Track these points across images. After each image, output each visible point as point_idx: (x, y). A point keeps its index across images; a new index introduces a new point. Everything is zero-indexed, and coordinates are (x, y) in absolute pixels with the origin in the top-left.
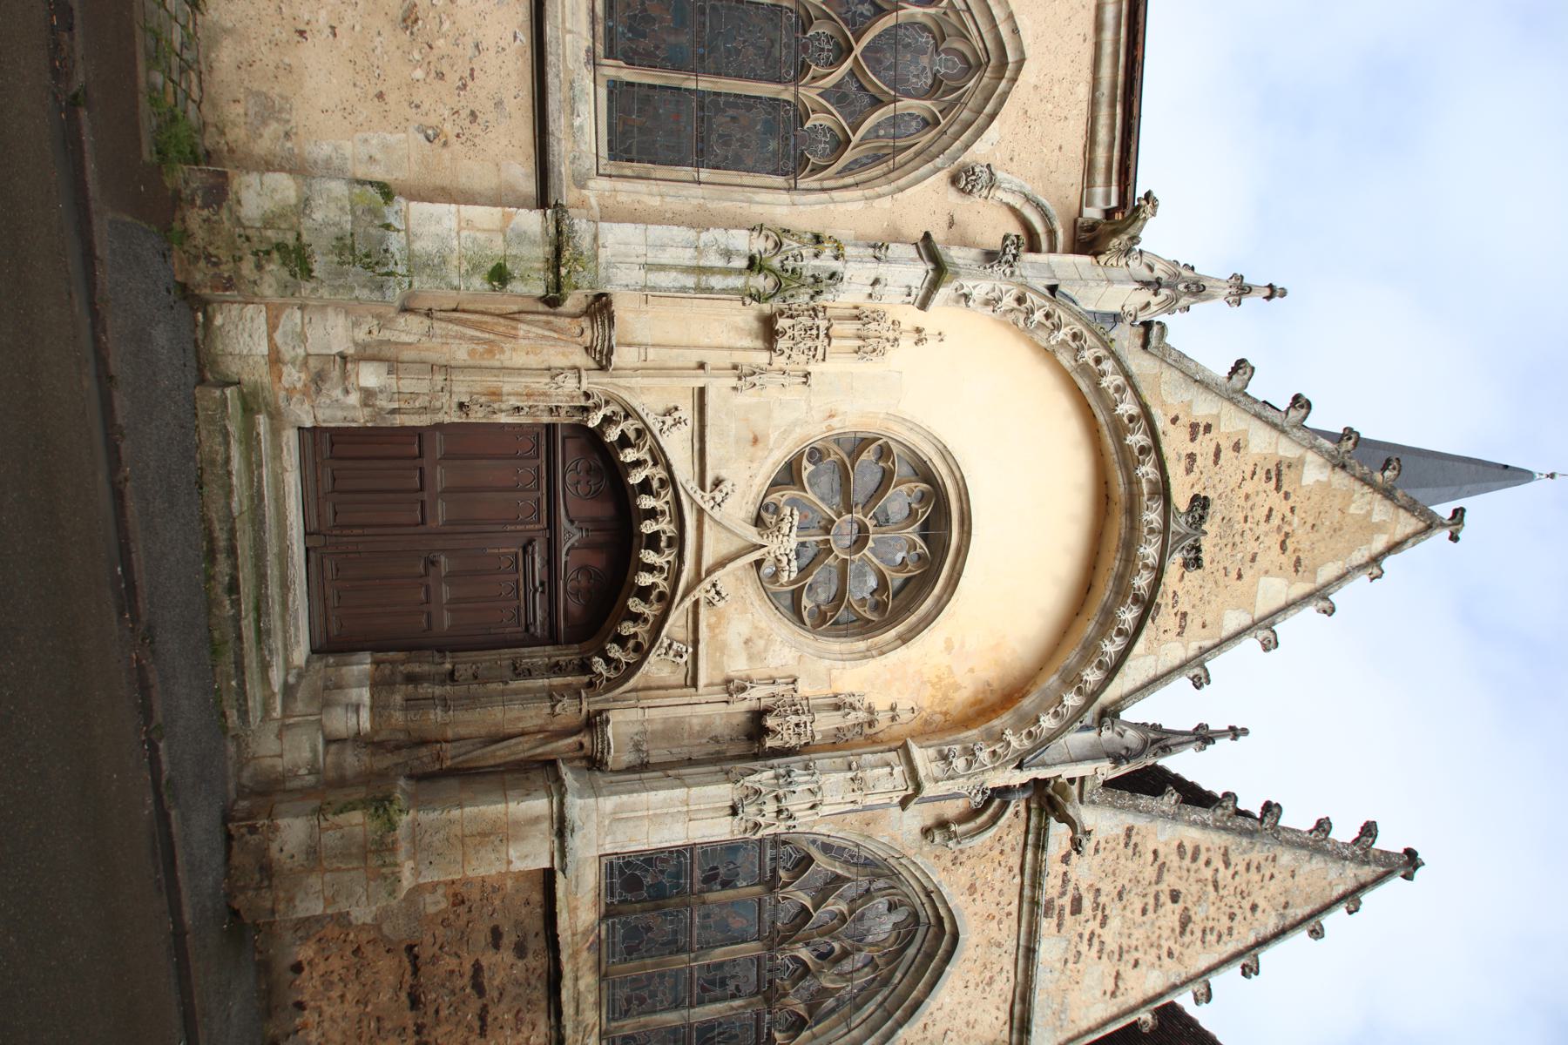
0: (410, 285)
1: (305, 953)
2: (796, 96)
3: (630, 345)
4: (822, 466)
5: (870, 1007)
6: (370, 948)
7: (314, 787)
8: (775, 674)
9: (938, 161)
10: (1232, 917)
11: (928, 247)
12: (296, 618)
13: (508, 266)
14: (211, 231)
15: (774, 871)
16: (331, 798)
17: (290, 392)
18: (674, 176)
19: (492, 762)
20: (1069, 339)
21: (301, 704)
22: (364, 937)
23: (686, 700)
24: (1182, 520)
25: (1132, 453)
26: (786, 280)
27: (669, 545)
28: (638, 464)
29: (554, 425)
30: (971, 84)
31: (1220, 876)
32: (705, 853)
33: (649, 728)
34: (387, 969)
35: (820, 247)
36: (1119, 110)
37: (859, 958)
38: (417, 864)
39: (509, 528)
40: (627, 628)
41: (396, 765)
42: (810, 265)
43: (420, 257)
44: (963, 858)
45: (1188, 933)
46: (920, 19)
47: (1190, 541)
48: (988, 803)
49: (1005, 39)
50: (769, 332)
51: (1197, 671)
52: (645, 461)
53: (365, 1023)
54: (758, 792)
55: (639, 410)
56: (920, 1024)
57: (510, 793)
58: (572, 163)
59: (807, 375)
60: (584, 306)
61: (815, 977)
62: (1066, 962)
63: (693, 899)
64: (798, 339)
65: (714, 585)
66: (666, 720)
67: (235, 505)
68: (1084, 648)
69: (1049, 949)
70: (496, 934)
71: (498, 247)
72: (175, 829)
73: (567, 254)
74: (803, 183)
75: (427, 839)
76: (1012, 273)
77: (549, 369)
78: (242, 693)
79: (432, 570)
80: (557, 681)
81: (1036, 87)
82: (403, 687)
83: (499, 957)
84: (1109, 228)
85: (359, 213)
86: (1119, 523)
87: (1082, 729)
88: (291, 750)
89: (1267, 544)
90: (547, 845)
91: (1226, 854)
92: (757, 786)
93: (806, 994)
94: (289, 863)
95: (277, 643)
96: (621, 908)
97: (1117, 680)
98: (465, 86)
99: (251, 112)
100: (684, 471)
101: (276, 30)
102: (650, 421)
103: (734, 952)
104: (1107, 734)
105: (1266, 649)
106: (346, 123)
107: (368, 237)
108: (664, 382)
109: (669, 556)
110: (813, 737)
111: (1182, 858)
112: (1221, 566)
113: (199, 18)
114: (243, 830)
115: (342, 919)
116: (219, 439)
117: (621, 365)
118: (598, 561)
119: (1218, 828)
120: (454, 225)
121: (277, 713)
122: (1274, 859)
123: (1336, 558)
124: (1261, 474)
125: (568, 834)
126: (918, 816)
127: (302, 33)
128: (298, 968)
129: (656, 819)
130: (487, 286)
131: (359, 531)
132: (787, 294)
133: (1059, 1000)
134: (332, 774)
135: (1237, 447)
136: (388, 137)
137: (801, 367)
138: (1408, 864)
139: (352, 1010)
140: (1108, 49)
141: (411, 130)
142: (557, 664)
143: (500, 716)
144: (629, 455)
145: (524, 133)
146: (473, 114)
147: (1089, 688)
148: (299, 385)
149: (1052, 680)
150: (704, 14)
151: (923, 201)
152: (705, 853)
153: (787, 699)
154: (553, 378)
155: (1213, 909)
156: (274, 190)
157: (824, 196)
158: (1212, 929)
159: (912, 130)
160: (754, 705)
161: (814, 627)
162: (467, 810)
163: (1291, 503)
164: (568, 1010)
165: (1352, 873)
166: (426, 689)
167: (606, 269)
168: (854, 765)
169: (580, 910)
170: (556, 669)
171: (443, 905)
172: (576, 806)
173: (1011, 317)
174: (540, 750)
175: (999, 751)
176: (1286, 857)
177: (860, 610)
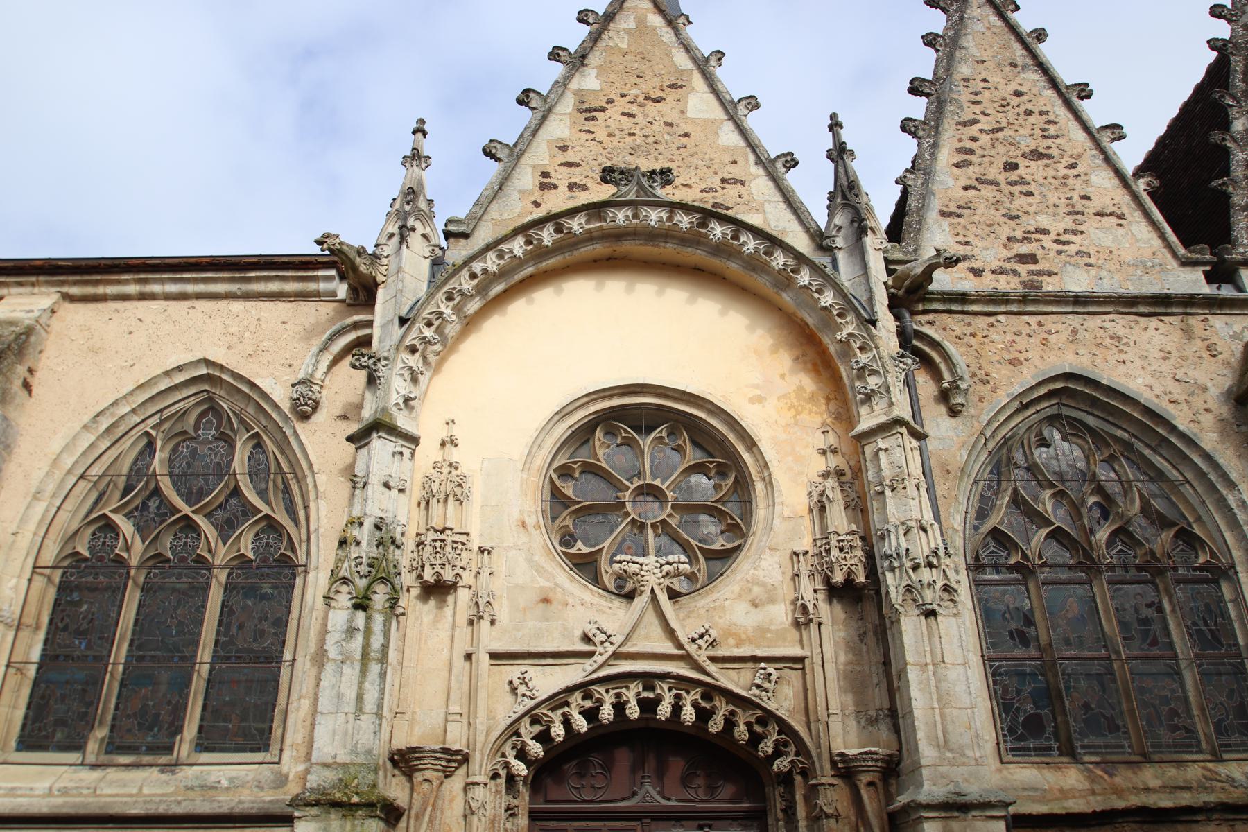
2: (224, 567)
3: (445, 731)
4: (578, 533)
5: (1158, 461)
8: (790, 574)
9: (289, 432)
10: (1029, 113)
11: (359, 439)
15: (1011, 569)
20: (451, 304)
23: (818, 669)
24: (624, 189)
25: (562, 239)
27: (653, 689)
28: (567, 722)
29: (531, 812)
30: (225, 406)
31: (986, 127)
32: (994, 645)
33: (851, 708)
35: (349, 541)
36: (253, 274)
37: (1105, 474)
40: (741, 733)
42: (366, 550)
44: (981, 374)
45: (1050, 152)
46: (166, 454)
47: (645, 181)
48: (917, 352)
49: (187, 377)
50: (437, 590)
51: (779, 165)
52: (564, 714)
54: (909, 589)
55: (510, 721)
56: (1171, 408)
58: (262, 789)
59: (481, 550)
60: (403, 779)
61: (1129, 521)
62: (1089, 265)
64: (443, 560)
65: (693, 640)
68: (754, 270)
69: (1077, 282)
74: (302, 559)
76: (386, 359)
77: (465, 816)
80: (801, 811)
81: (229, 348)
84: (351, 274)
86: (628, 246)
87: (835, 267)
89: (655, 114)
90: (979, 824)
91: (964, 124)
92: (901, 590)
93: (1151, 530)
97: (789, 240)
100: (574, 673)
102: (521, 710)
103: (1107, 611)
104: (839, 242)
105: (757, 106)
108: (482, 695)
109: (663, 688)
110: (852, 533)
111: (970, 163)
117: (464, 741)
118: (677, 766)
119: (937, 132)
122: (966, 80)
123: (669, 55)
124: (589, 125)
125: (963, 799)
126: (938, 424)
132: (392, 570)
133: (1132, 270)
135: (564, 148)
137: (474, 555)
140: (201, 288)
144: (558, 731)
147: (791, 262)
149: (786, 298)
151: (321, 443)
152: (994, 645)
153: (815, 561)
154: (473, 813)
155: (1021, 131)
157: (313, 537)
158: (1043, 130)
159: (261, 457)
160: (821, 596)
164: (1185, 799)
167: (357, 754)
168: (879, 488)
172: (930, 789)
173: (432, 359)
175: (859, 343)
176: (964, 70)
177: (725, 490)
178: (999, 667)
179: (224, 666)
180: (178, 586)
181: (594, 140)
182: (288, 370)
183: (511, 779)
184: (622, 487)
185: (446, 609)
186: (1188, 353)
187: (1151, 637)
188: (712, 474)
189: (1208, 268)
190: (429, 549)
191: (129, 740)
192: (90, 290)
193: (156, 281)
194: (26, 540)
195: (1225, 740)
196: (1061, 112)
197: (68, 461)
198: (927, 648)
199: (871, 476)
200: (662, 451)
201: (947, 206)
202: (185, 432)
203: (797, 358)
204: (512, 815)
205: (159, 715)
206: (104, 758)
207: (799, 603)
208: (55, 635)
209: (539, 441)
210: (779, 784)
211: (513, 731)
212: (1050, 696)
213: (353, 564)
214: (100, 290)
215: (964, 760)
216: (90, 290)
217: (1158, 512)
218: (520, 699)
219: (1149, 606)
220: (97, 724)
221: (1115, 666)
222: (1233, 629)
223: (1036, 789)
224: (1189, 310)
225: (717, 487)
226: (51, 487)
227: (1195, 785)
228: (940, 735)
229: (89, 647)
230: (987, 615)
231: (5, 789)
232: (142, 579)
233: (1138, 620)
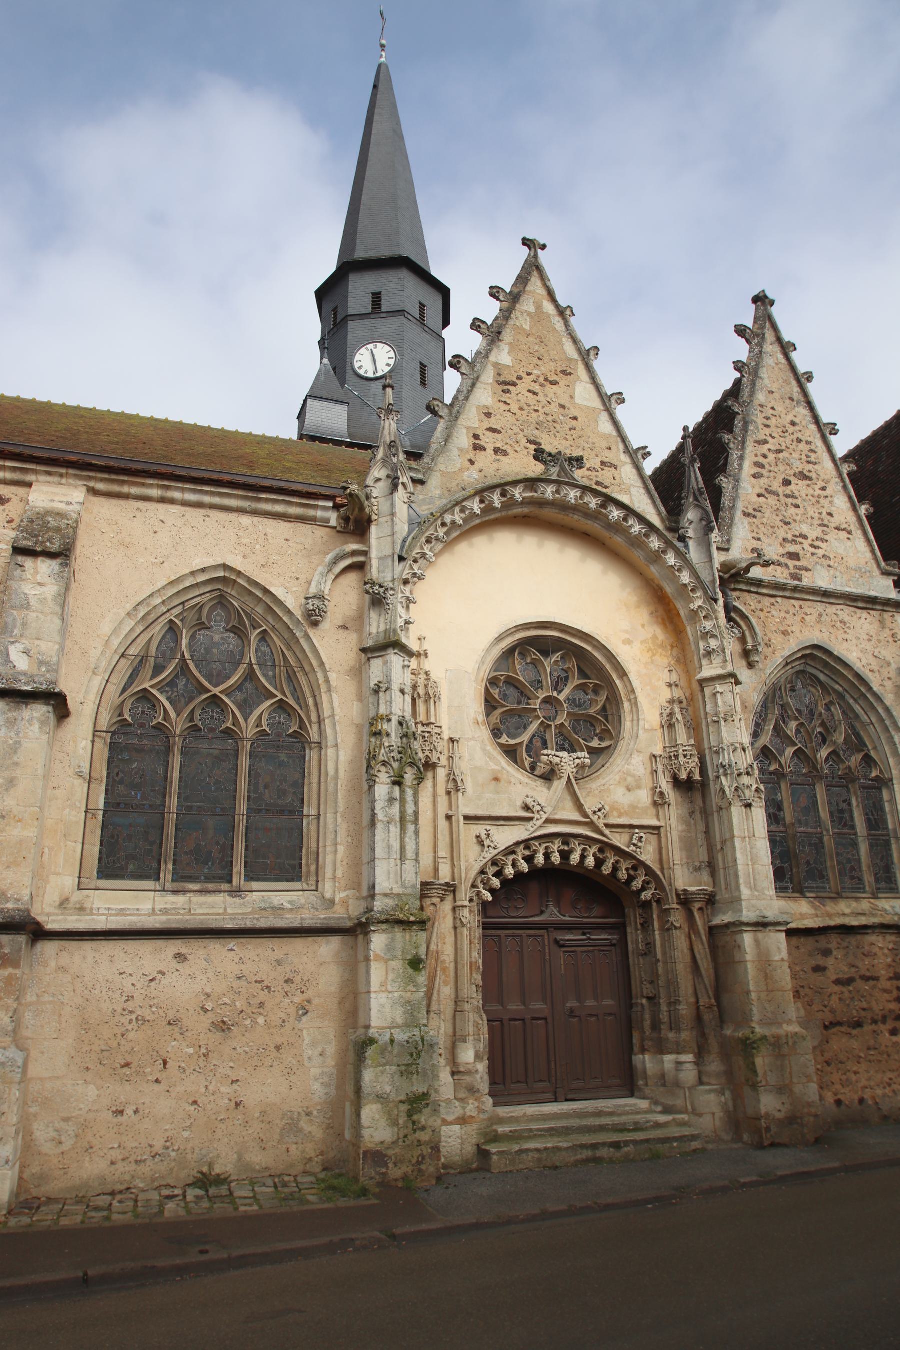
6: (826, 1054)
8: (649, 770)
10: (799, 441)
12: (620, 1106)
13: (409, 957)
14: (402, 1162)
18: (314, 834)
21: (679, 1098)
26: (407, 758)
27: (567, 844)
31: (773, 448)
34: (840, 1043)
36: (264, 496)
39: (547, 957)
40: (623, 875)
42: (394, 740)
43: (406, 1019)
44: (766, 641)
47: (566, 464)
49: (208, 578)
54: (737, 789)
57: (737, 959)
58: (317, 910)
59: (452, 740)
62: (829, 566)
63: (790, 832)
65: (595, 813)
66: (681, 850)
67: (565, 1145)
68: (632, 545)
69: (821, 579)
70: (818, 969)
71: (397, 964)
72: (788, 1172)
74: (314, 736)
76: (392, 589)
77: (455, 928)
78: (681, 1139)
81: (244, 557)
82: (663, 1032)
83: (831, 967)
88: (710, 1107)
90: (772, 935)
92: (733, 789)
97: (648, 517)
98: (268, 987)
100: (519, 833)
102: (489, 857)
104: (691, 533)
105: (623, 401)
106: (298, 1073)
109: (575, 845)
110: (692, 746)
111: (762, 476)
112: (569, 433)
113: (233, 1178)
114: (768, 1136)
116: (524, 1156)
120: (384, 995)
121: (685, 1117)
122: (762, 406)
123: (560, 343)
124: (505, 397)
125: (766, 920)
126: (744, 674)
127: (238, 1105)
128: (839, 1103)
129: (754, 860)
130: (423, 973)
133: (853, 573)
136: (306, 1042)
137: (446, 744)
138: (764, 304)
140: (217, 500)
141: (300, 1026)
142: (642, 925)
143: (682, 968)
145: (299, 945)
148: (477, 1104)
149: (654, 571)
151: (333, 648)
154: (463, 925)
155: (794, 455)
156: (373, 1119)
158: (807, 456)
160: (670, 786)
161: (612, 738)
162: (752, 988)
163: (524, 375)
164: (863, 921)
165: (771, 348)
166: (664, 1017)
169: (803, 912)
170: (646, 926)
172: (748, 915)
174: (704, 938)
175: (704, 614)
181: (509, 411)
182: (296, 582)
184: (532, 696)
186: (882, 638)
189: (896, 578)
192: (116, 488)
193: (177, 489)
196: (819, 444)
201: (747, 508)
203: (652, 614)
205: (211, 852)
214: (125, 489)
216: (116, 488)
218: (486, 849)
224: (885, 609)
226: (104, 664)
228: (752, 881)
229: (143, 798)
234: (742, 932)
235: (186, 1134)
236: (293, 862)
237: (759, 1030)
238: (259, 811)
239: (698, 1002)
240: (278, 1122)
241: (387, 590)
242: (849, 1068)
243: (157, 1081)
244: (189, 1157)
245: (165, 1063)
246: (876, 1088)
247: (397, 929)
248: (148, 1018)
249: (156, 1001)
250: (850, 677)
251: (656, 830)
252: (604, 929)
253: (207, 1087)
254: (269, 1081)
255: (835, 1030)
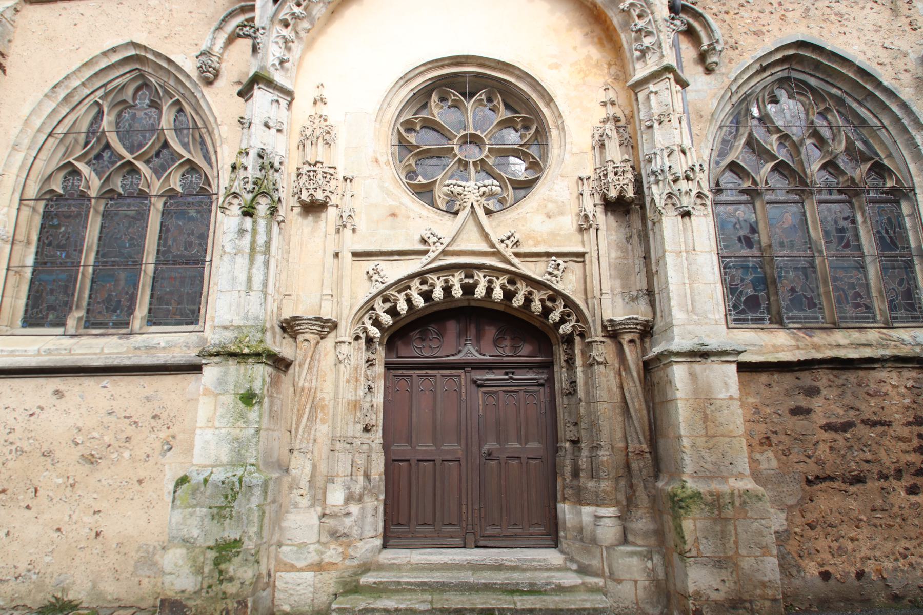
0: (253, 465)
1: (812, 569)
5: (862, 112)
6: (808, 515)
7: (664, 556)
8: (576, 194)
9: (199, 96)
11: (245, 93)
12: (525, 560)
13: (242, 392)
16: (672, 544)
17: (345, 556)
19: (645, 412)
22: (798, 520)
23: (595, 261)
27: (472, 277)
28: (409, 300)
32: (726, 247)
33: (619, 290)
34: (827, 502)
35: (238, 166)
38: (732, 475)
39: (464, 397)
40: (536, 307)
41: (645, 488)
42: (253, 172)
46: (112, 118)
50: (313, 208)
52: (407, 295)
53: (877, 522)
54: (670, 196)
55: (367, 299)
57: (669, 397)
58: (189, 348)
59: (345, 180)
60: (291, 340)
61: (836, 157)
65: (502, 241)
70: (797, 411)
71: (229, 400)
73: (233, 348)
75: (709, 466)
76: (263, 28)
79: (495, 455)
80: (579, 361)
81: (150, 33)
82: (582, 480)
83: (818, 410)
85: (195, 502)
88: (633, 571)
92: (664, 196)
94: (730, 584)
95: (541, 578)
96: (774, 312)
98: (135, 423)
99: (148, 573)
100: (414, 265)
101: (95, 552)
102: (375, 291)
103: (814, 222)
107: (212, 496)
108: (346, 282)
110: (626, 161)
113: (84, 605)
115: (782, 537)
117: (334, 314)
118: (491, 332)
120: (211, 431)
121: (600, 581)
125: (705, 349)
128: (826, 576)
130: (256, 408)
131: (464, 507)
134: (652, 541)
136: (167, 477)
139: (865, 532)
141: (163, 461)
142: (567, 361)
144: (402, 307)
146: (154, 417)
148: (340, 550)
150: (106, 262)
151: (220, 101)
152: (726, 247)
153: (595, 184)
156: (176, 565)
160: (600, 209)
162: (682, 432)
164: (867, 353)
166: (583, 463)
167: (248, 320)
168: (649, 123)
170: (570, 362)
171: (770, 454)
172: (680, 341)
174: (635, 374)
175: (638, 11)
177: (528, 137)
178: (729, 262)
179: (164, 267)
180: (129, 212)
183: (370, 341)
184: (452, 137)
185: (321, 223)
187: (845, 241)
188: (519, 127)
190: (304, 178)
191: (100, 319)
194: (11, 179)
195: (894, 314)
197: (38, 123)
198: (682, 240)
199: (642, 115)
200: (482, 111)
202: (124, 101)
203: (587, 34)
204: (371, 365)
205: (120, 301)
206: (82, 331)
207: (582, 214)
208: (43, 248)
209: (388, 100)
210: (563, 343)
211: (369, 307)
212: (766, 282)
213: (242, 183)
215: (706, 321)
217: (859, 149)
218: (374, 284)
219: (845, 219)
220: (74, 308)
221: (817, 262)
222: (907, 236)
223: (755, 345)
225: (521, 137)
226: (26, 142)
227: (874, 343)
228: (689, 303)
229: (67, 256)
230: (721, 226)
231: (8, 351)
232: (101, 208)
233: (837, 229)
234: (671, 363)
235: (47, 559)
236: (192, 307)
237: (692, 485)
238: (166, 262)
239: (627, 448)
240: (133, 554)
241: (258, 30)
242: (843, 533)
243: (28, 507)
244: (47, 580)
245: (36, 491)
246: (884, 559)
247: (232, 362)
248: (25, 449)
249: (33, 434)
250: (850, 75)
251: (580, 256)
252: (531, 368)
253: (70, 516)
254: (129, 513)
255: (823, 486)
